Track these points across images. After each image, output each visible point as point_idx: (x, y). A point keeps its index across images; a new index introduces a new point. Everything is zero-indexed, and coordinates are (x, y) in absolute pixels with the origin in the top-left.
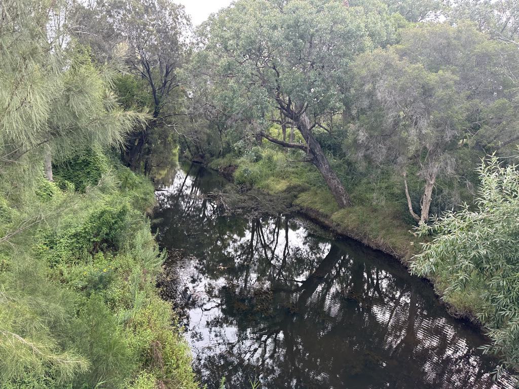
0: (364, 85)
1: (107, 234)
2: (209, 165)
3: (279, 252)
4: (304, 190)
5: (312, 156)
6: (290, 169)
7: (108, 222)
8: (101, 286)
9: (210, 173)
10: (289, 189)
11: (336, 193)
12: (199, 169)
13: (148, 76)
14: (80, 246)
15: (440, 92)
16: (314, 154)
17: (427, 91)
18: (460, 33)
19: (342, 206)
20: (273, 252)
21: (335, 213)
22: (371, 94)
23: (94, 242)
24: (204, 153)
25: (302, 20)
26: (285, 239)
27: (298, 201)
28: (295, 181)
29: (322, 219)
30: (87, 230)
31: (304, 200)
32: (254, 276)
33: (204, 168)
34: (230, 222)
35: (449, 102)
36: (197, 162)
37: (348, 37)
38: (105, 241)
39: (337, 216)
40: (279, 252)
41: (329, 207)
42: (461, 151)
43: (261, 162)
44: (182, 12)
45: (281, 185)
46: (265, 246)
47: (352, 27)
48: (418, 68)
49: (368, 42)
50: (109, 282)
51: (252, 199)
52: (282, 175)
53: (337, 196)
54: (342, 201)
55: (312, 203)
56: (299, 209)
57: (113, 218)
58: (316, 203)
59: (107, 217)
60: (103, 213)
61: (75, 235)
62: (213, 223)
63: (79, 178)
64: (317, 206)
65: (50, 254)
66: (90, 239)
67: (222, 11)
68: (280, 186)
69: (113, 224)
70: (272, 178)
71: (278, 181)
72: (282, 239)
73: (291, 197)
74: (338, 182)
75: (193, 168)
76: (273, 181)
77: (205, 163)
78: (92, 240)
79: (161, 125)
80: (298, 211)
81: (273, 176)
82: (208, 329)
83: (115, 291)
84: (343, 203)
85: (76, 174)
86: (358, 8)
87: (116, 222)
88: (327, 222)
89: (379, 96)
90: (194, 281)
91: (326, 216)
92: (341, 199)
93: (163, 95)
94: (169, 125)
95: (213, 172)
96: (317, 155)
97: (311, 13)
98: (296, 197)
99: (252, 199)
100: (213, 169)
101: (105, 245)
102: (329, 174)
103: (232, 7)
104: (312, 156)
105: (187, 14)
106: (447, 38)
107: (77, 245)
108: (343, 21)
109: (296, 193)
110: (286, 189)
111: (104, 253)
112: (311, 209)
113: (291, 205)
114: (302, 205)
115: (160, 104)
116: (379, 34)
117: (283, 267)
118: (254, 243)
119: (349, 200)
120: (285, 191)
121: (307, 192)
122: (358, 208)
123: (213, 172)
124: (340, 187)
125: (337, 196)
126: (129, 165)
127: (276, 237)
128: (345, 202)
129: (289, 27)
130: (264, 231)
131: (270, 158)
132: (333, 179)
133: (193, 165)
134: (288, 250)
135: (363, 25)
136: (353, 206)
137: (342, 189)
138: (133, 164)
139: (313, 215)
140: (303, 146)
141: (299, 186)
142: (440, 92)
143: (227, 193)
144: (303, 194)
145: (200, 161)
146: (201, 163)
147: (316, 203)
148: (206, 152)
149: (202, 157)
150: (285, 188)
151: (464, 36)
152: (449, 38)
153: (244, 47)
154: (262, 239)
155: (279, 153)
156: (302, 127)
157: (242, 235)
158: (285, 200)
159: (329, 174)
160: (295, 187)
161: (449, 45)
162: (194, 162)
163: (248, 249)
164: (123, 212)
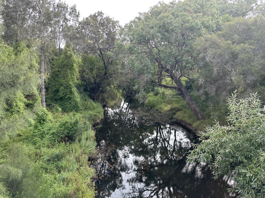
0: (199, 54)
1: (67, 133)
2: (134, 97)
3: (172, 143)
4: (179, 110)
5: (180, 92)
6: (174, 99)
7: (68, 127)
8: (56, 160)
9: (135, 102)
10: (171, 110)
11: (195, 112)
12: (130, 99)
13: (101, 56)
14: (55, 139)
15: (241, 56)
16: (181, 91)
17: (234, 56)
18: (256, 22)
19: (198, 119)
20: (168, 143)
21: (195, 123)
22: (204, 59)
23: (61, 137)
24: (132, 91)
25: (166, 22)
26: (170, 138)
27: (175, 116)
28: (175, 105)
29: (188, 126)
30: (58, 131)
31: (179, 116)
32: (158, 156)
33: (132, 99)
34: (144, 128)
35: (250, 60)
36: (129, 96)
37: (192, 29)
38: (66, 136)
39: (195, 125)
40: (172, 143)
41: (191, 120)
42: (259, 88)
43: (159, 96)
44: (118, 24)
45: (167, 107)
46: (164, 140)
47: (194, 24)
48: (228, 44)
49: (204, 31)
50: (62, 158)
51: (152, 115)
52: (169, 103)
53: (196, 113)
54: (198, 116)
55: (183, 117)
56: (176, 120)
57: (71, 126)
58: (185, 117)
59: (68, 125)
60: (66, 122)
61: (53, 134)
62: (155, 127)
63: (66, 105)
64: (186, 119)
65: (40, 142)
66: (59, 135)
67: (131, 22)
68: (167, 108)
69: (71, 128)
70: (164, 104)
71: (167, 105)
72: (172, 136)
73: (172, 114)
74: (195, 106)
75: (127, 99)
76: (164, 105)
77: (133, 96)
78: (60, 136)
79: (108, 79)
80: (176, 121)
81: (165, 103)
82: (128, 184)
83: (63, 163)
84: (199, 117)
85: (65, 103)
86: (198, 14)
87: (73, 127)
88: (190, 128)
89: (207, 59)
90: (125, 157)
91: (190, 125)
92: (198, 115)
93: (108, 64)
94: (111, 79)
95: (136, 101)
96: (183, 91)
97: (171, 19)
98: (175, 114)
99: (152, 115)
100: (136, 100)
101: (67, 138)
102: (190, 101)
103: (136, 20)
104: (180, 92)
105: (120, 25)
106: (247, 25)
107: (53, 139)
108: (188, 21)
109: (175, 112)
110: (170, 110)
111: (66, 143)
112: (182, 120)
113: (172, 118)
114: (178, 118)
115: (107, 69)
116: (212, 27)
117: (173, 151)
118: (159, 138)
119: (202, 116)
120: (169, 111)
121: (181, 111)
122: (207, 121)
123: (136, 101)
124: (197, 109)
125: (196, 113)
126: (92, 99)
127: (169, 135)
128: (200, 117)
129: (160, 27)
130: (163, 132)
131: (163, 94)
132: (192, 104)
133: (127, 97)
134: (176, 142)
135: (199, 23)
136: (205, 119)
137: (198, 110)
138: (95, 98)
139: (183, 124)
140: (175, 87)
141: (177, 108)
142: (241, 56)
143: (138, 112)
144: (179, 112)
145: (130, 96)
146: (131, 96)
147: (185, 117)
148: (133, 91)
149: (131, 93)
150: (169, 109)
151: (259, 23)
152: (248, 25)
153: (137, 39)
154: (162, 136)
155: (170, 90)
156: (173, 77)
157: (152, 133)
158: (169, 116)
159: (190, 101)
160: (175, 109)
161: (249, 29)
162: (127, 96)
163: (155, 141)
164: (76, 122)
